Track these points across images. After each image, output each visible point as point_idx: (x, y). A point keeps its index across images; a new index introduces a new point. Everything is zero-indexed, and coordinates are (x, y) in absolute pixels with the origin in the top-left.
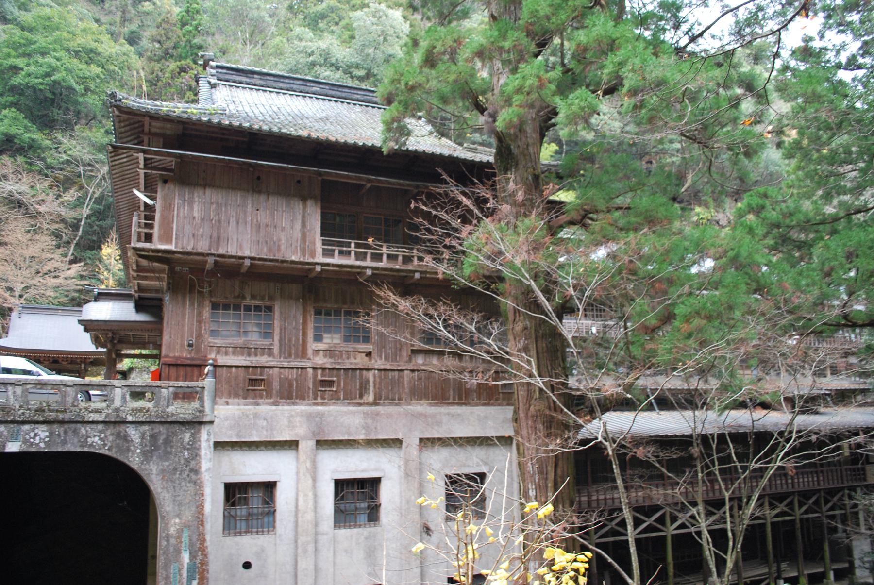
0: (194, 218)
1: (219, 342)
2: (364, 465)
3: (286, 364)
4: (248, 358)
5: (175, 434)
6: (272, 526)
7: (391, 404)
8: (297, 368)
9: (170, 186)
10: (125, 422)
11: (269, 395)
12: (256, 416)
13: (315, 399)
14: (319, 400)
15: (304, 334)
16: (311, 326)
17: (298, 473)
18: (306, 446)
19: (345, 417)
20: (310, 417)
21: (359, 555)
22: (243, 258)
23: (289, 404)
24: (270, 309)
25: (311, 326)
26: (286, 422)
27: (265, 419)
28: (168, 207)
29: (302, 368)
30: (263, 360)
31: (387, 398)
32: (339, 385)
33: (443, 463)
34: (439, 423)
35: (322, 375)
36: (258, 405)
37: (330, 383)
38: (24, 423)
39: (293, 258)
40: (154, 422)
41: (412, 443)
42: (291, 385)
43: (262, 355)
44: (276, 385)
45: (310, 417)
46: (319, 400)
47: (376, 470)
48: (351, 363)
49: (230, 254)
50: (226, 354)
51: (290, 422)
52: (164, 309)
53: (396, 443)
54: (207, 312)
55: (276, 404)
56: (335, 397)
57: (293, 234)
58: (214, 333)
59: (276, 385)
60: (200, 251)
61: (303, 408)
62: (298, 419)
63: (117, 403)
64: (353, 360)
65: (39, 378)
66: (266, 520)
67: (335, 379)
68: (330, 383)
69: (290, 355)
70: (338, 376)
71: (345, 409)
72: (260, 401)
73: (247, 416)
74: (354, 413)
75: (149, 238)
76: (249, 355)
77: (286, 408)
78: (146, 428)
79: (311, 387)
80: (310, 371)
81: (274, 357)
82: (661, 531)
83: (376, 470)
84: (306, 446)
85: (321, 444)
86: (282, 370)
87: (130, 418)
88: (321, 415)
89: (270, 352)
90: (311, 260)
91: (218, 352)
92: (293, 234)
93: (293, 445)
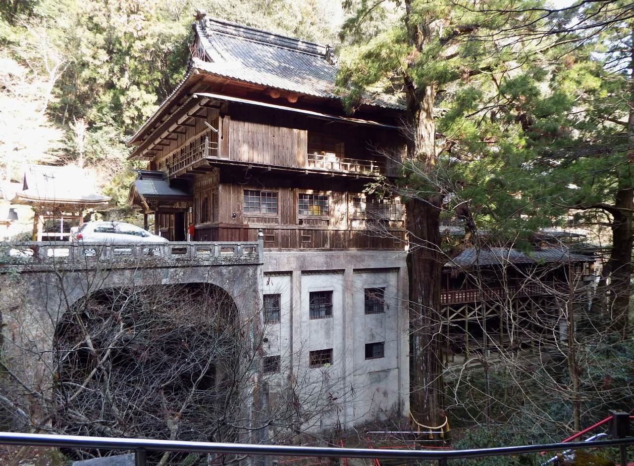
1: (249, 214)
2: (324, 284)
3: (285, 228)
5: (244, 271)
6: (279, 318)
7: (339, 250)
9: (226, 120)
11: (277, 246)
14: (302, 248)
16: (297, 204)
17: (292, 289)
18: (297, 273)
19: (316, 258)
20: (298, 258)
21: (322, 333)
23: (287, 251)
24: (276, 195)
26: (286, 260)
30: (273, 225)
31: (336, 247)
32: (312, 240)
33: (362, 282)
34: (363, 261)
36: (271, 251)
37: (307, 238)
39: (293, 166)
41: (349, 270)
42: (287, 240)
44: (280, 239)
45: (298, 258)
46: (302, 248)
47: (330, 286)
50: (253, 221)
52: (220, 196)
53: (342, 271)
56: (310, 246)
57: (293, 148)
58: (247, 209)
59: (280, 239)
63: (216, 255)
66: (274, 315)
68: (307, 238)
69: (287, 222)
70: (312, 235)
74: (319, 255)
75: (213, 152)
76: (265, 222)
77: (285, 252)
78: (231, 268)
80: (297, 231)
82: (463, 317)
83: (330, 286)
84: (297, 273)
85: (305, 272)
87: (223, 263)
88: (304, 257)
89: (277, 221)
91: (249, 221)
92: (293, 148)
93: (289, 273)
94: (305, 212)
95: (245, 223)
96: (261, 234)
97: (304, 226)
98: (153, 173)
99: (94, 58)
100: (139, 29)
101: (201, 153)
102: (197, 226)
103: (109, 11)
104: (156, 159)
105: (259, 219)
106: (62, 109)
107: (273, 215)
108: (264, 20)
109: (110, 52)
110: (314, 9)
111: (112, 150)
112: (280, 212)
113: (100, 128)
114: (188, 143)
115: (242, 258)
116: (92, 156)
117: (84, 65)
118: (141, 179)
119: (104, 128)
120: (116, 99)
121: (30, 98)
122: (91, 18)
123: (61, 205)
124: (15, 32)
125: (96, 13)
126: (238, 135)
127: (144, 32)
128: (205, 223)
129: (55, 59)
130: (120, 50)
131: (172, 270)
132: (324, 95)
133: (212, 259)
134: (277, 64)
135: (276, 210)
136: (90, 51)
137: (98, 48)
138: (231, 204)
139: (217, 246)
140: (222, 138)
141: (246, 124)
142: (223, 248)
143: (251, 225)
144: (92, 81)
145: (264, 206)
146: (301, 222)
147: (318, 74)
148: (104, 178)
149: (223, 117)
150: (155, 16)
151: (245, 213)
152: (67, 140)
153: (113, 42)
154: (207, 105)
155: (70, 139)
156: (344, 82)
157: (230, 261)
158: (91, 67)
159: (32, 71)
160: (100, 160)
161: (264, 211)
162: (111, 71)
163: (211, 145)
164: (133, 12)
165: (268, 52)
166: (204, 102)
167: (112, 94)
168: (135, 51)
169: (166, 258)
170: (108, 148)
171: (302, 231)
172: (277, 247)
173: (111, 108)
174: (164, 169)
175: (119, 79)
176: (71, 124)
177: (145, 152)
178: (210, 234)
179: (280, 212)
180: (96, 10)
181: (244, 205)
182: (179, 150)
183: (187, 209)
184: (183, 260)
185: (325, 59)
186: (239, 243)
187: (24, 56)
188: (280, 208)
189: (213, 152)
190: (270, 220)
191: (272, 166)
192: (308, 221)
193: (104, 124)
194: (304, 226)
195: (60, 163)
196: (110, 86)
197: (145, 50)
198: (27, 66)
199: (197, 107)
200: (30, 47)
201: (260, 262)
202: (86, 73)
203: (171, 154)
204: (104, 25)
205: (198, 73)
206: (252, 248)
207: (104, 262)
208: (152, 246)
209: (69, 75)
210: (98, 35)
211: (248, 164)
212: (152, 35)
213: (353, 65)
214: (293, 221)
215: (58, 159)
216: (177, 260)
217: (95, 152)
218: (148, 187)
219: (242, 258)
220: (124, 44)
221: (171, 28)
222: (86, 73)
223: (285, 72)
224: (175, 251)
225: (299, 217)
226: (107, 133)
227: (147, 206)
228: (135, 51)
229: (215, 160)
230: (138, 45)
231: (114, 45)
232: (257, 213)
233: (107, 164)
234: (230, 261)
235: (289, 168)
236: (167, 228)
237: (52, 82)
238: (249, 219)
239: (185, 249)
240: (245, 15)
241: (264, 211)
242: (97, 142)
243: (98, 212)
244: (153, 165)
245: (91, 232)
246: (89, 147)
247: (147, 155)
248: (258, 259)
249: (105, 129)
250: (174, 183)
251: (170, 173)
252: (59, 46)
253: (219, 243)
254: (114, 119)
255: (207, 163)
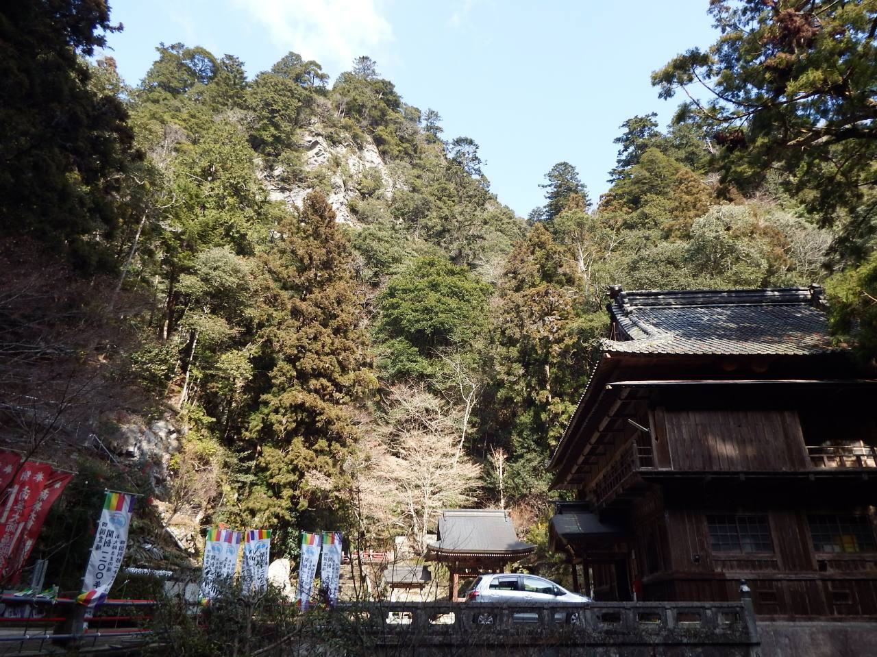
0: (684, 440)
1: (722, 555)
3: (793, 577)
4: (753, 572)
8: (805, 580)
9: (659, 414)
10: (680, 644)
11: (783, 611)
12: (777, 633)
13: (832, 613)
14: (787, 572)
15: (805, 544)
16: (809, 535)
20: (832, 635)
22: (737, 473)
25: (809, 535)
26: (807, 638)
27: (786, 636)
28: (660, 430)
29: (810, 580)
30: (768, 572)
35: (834, 587)
38: (597, 645)
39: (784, 469)
40: (706, 644)
43: (767, 567)
45: (832, 635)
46: (836, 615)
48: (862, 574)
49: (723, 470)
50: (732, 567)
51: (812, 639)
54: (705, 526)
55: (792, 619)
58: (716, 547)
60: (696, 470)
61: (822, 624)
62: (820, 636)
63: (671, 624)
64: (862, 570)
65: (560, 598)
67: (848, 591)
71: (867, 625)
72: (776, 616)
73: (768, 633)
75: (647, 462)
76: (754, 567)
77: (803, 623)
79: (824, 600)
80: (820, 583)
81: (779, 569)
86: (790, 583)
87: (685, 641)
88: (845, 633)
89: (774, 565)
90: (802, 470)
94: (828, 548)
95: (719, 570)
96: (746, 588)
97: (830, 571)
98: (580, 507)
99: (509, 374)
100: (554, 330)
101: (629, 465)
102: (645, 579)
103: (522, 319)
104: (584, 487)
105: (743, 564)
106: (481, 440)
107: (764, 555)
108: (712, 282)
109: (526, 366)
110: (787, 252)
111: (536, 483)
112: (777, 549)
113: (522, 456)
114: (618, 457)
115: (717, 631)
116: (513, 492)
117: (500, 384)
118: (561, 513)
119: (525, 455)
120: (537, 416)
121: (447, 431)
122: (503, 332)
123: (478, 559)
124: (432, 365)
125: (508, 325)
126: (680, 432)
127: (561, 333)
128: (656, 574)
129: (472, 383)
130: (536, 360)
131: (600, 650)
132: (814, 351)
133: (664, 633)
134: (734, 326)
135: (769, 546)
136: (504, 368)
137: (512, 362)
138: (688, 542)
139: (670, 610)
140: (657, 439)
141: (691, 416)
142: (681, 616)
143: (730, 574)
144: (508, 401)
145: (748, 541)
146: (823, 565)
147: (806, 326)
148: (528, 520)
149: (653, 410)
150: (573, 312)
151: (714, 553)
152: (485, 476)
153: (528, 353)
154: (630, 396)
155: (489, 474)
156: (844, 325)
157: (695, 636)
158: (507, 385)
159: (448, 403)
160: (523, 496)
161: (748, 550)
162: (528, 385)
163: (640, 451)
164: (547, 314)
165: (721, 315)
166: (625, 394)
167: (532, 413)
168: (553, 357)
169: (590, 629)
170: (532, 481)
171: (829, 584)
172: (785, 613)
173: (531, 430)
174: (591, 498)
175: (538, 394)
176: (489, 456)
177: (569, 477)
178: (664, 589)
179: (777, 549)
180: (508, 322)
181: (712, 541)
182: (609, 468)
183: (629, 554)
184: (615, 632)
185: (811, 305)
186: (707, 604)
187: (439, 387)
188: (776, 542)
189: (647, 462)
190: (761, 564)
191: (746, 473)
192: (836, 563)
193: (525, 450)
194: (830, 571)
195: (478, 505)
196: (529, 403)
197: (564, 353)
198: (443, 397)
199: (618, 403)
200: (446, 377)
201: (754, 640)
202: (501, 394)
203: (601, 476)
204: (518, 336)
205: (608, 356)
206: (735, 615)
207: (499, 633)
208: (570, 608)
209: (487, 396)
210: (512, 348)
211: (705, 473)
212: (570, 334)
213: (851, 297)
214: (807, 565)
215: (476, 499)
216: (608, 632)
217: (516, 488)
218: (571, 524)
219: (717, 631)
220: (540, 352)
221: (591, 321)
222: (501, 394)
223: (744, 335)
224: (606, 618)
225: (817, 557)
226: (529, 461)
227: (573, 552)
228: (553, 357)
229: (651, 473)
230: (556, 348)
231: (530, 355)
232: (735, 553)
233: (533, 502)
234: (695, 636)
235: (779, 473)
236: (608, 586)
237: (468, 409)
238: (724, 563)
239: (619, 614)
240: (683, 281)
241: (748, 549)
242: (519, 474)
243: (524, 568)
244: (581, 495)
245: (487, 588)
246: (510, 481)
247: (572, 482)
248: (747, 633)
249: (529, 456)
250: (604, 517)
251: (598, 501)
252: (473, 370)
253: (673, 604)
254: (537, 443)
255: (640, 478)
